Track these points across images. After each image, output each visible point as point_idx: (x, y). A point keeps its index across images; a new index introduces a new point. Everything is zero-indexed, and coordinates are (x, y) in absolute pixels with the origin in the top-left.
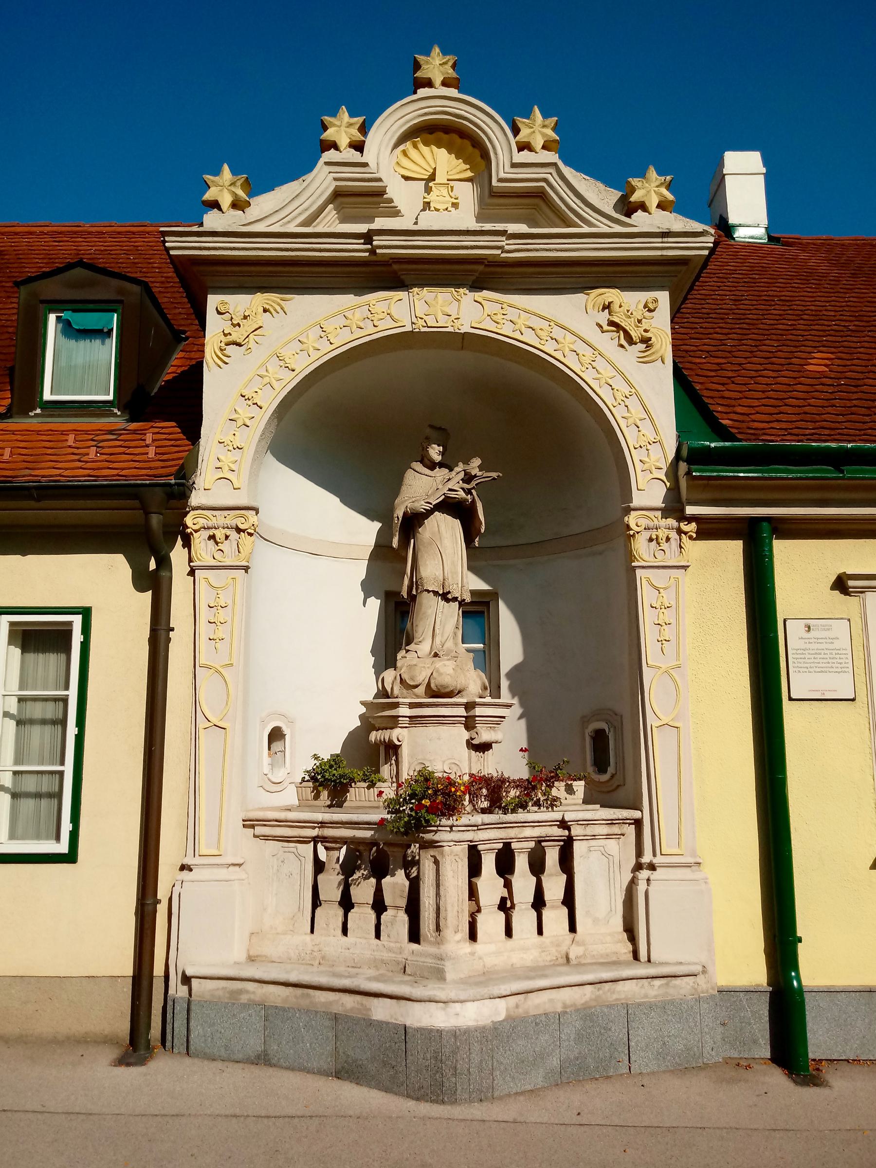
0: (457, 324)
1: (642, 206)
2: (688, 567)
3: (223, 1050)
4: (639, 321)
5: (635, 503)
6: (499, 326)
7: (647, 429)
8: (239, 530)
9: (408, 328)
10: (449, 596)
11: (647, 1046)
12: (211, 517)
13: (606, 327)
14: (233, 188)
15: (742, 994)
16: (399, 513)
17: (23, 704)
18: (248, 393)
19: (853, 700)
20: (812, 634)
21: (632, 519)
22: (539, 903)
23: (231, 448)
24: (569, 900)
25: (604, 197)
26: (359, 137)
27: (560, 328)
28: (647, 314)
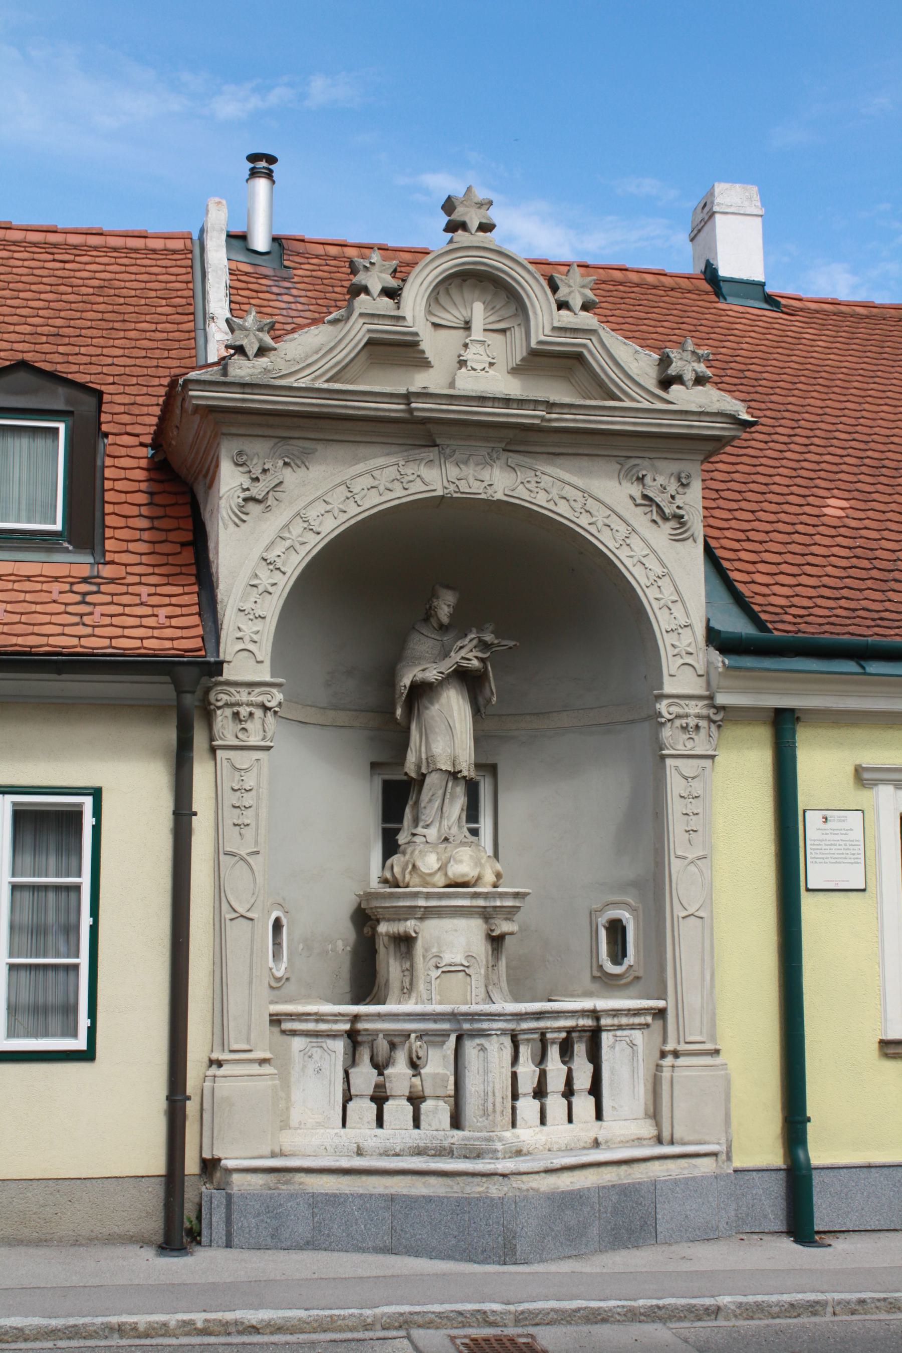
0: (490, 491)
1: (679, 379)
2: (715, 756)
3: (269, 1239)
4: (673, 497)
5: (668, 689)
6: (532, 495)
7: (677, 610)
8: (266, 709)
9: (439, 493)
10: (459, 776)
11: (671, 1219)
12: (235, 693)
13: (639, 501)
14: (261, 335)
15: (754, 1173)
16: (406, 681)
17: (18, 894)
18: (271, 556)
19: (864, 890)
20: (829, 825)
21: (663, 707)
22: (569, 1092)
23: (252, 617)
24: (595, 1090)
25: (640, 364)
26: (393, 283)
27: (597, 505)
28: (680, 490)
